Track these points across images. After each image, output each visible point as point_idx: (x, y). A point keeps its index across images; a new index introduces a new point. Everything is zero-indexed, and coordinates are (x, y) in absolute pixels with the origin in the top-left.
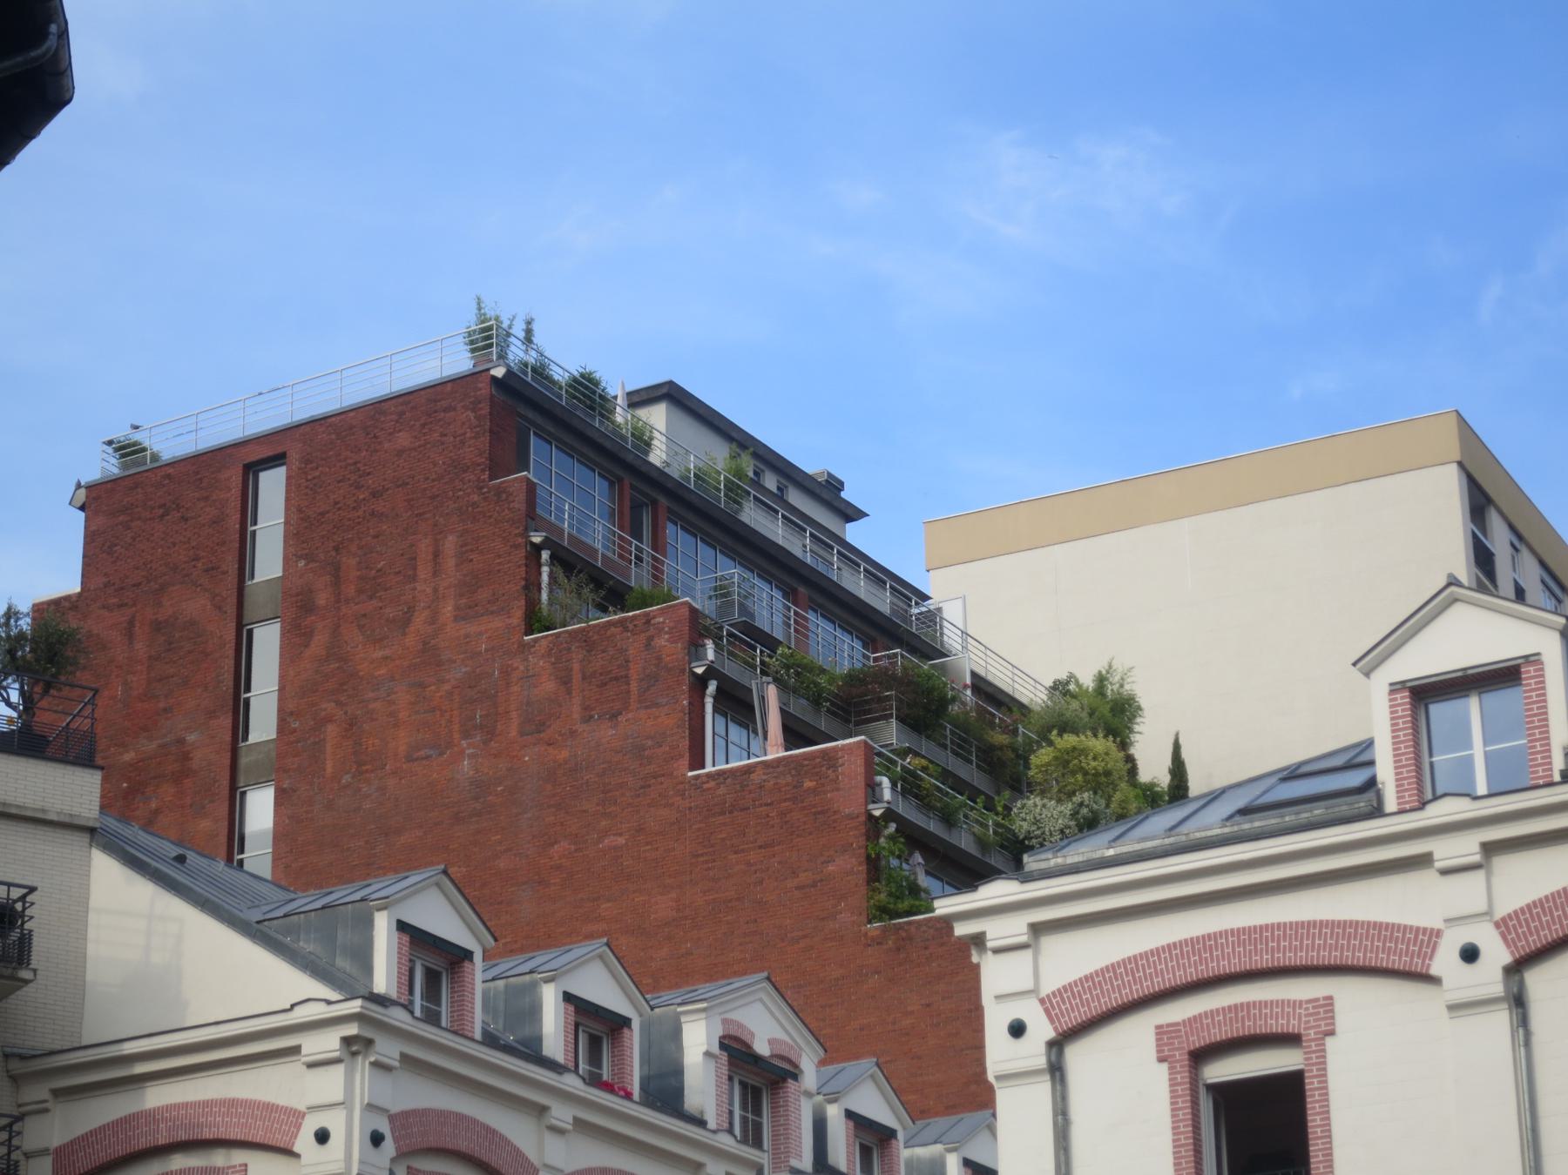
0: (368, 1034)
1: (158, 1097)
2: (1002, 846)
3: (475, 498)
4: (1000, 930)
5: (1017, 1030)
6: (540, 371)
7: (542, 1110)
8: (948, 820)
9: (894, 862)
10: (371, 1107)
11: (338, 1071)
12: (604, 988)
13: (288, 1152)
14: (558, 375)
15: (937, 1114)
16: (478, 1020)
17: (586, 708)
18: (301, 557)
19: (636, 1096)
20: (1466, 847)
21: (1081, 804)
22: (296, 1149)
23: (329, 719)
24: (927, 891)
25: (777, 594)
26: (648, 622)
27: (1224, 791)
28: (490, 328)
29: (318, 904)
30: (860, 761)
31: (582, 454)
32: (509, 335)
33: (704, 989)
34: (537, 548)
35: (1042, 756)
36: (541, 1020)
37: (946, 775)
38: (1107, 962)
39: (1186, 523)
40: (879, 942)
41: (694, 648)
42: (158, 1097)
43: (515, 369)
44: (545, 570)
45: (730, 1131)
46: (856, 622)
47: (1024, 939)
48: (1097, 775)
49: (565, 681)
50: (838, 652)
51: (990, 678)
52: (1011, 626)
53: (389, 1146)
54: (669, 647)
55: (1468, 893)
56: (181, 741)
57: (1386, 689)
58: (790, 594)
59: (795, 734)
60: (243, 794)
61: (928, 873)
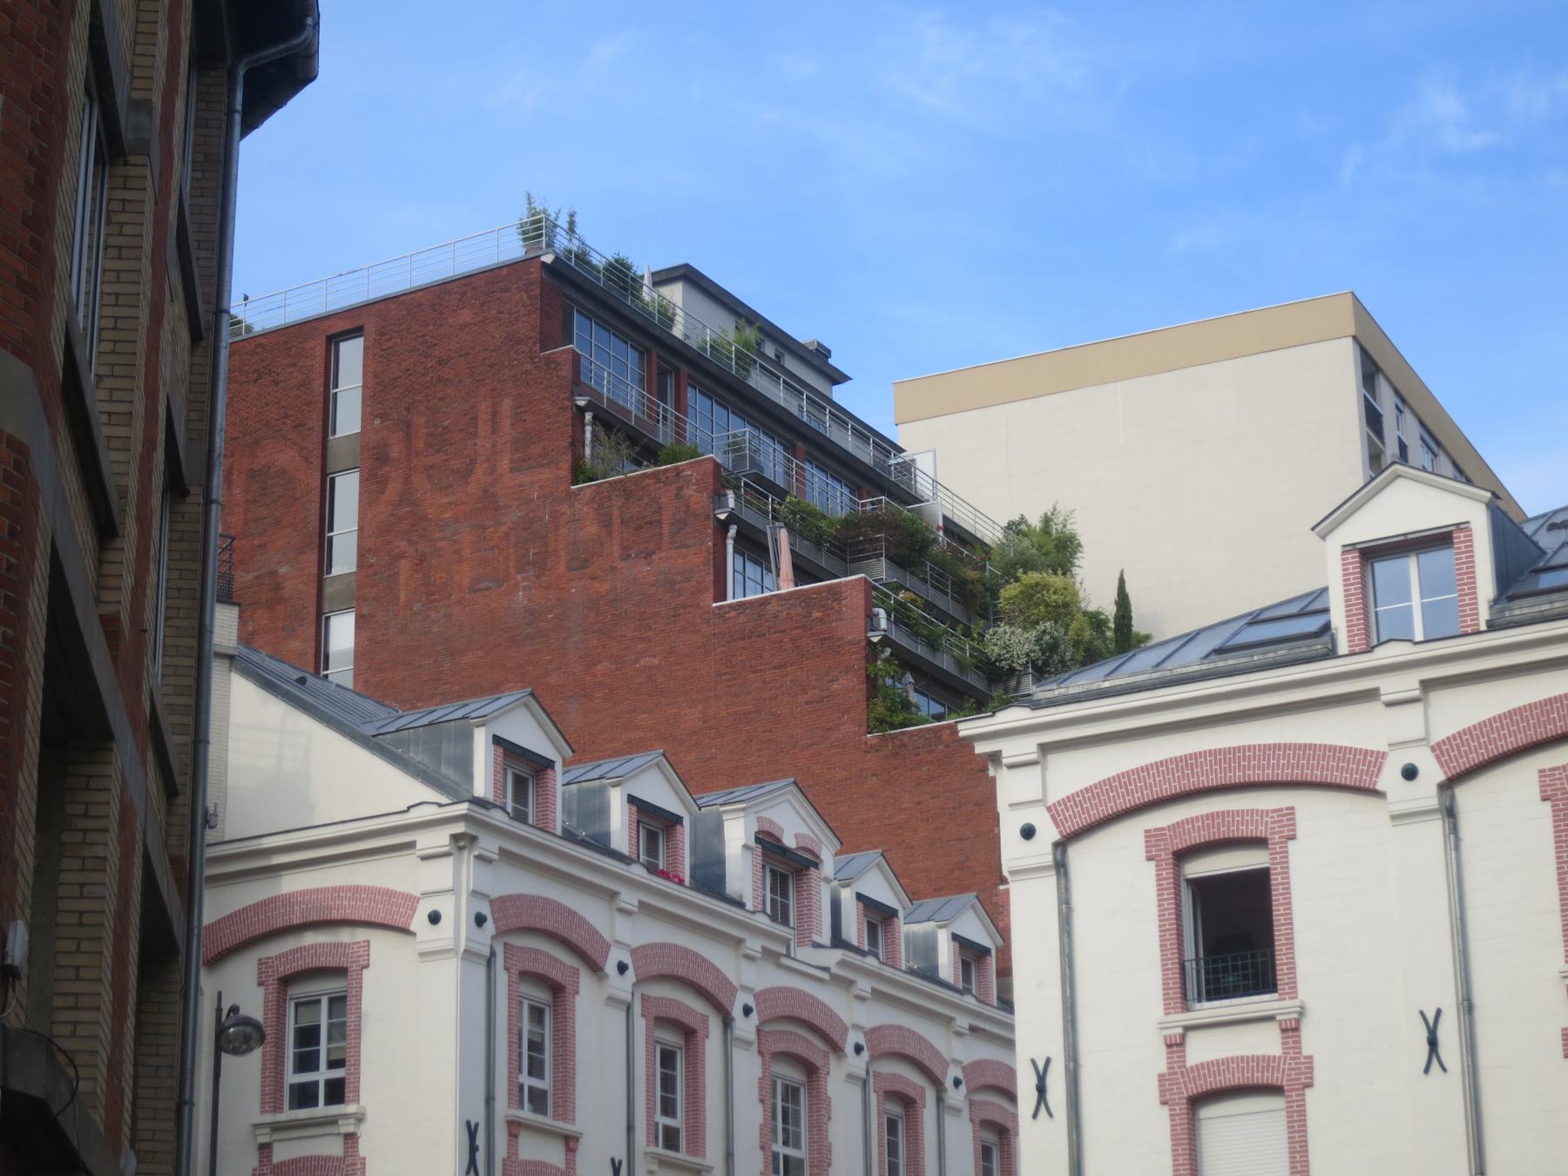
0: (473, 832)
1: (291, 884)
2: (977, 667)
3: (528, 367)
4: (1012, 750)
5: (1028, 833)
6: (582, 257)
7: (613, 895)
8: (933, 645)
9: (889, 681)
10: (475, 894)
11: (448, 863)
12: (661, 792)
13: (405, 931)
14: (597, 260)
15: (926, 896)
16: (559, 821)
17: (624, 548)
18: (377, 416)
19: (687, 882)
20: (1407, 684)
21: (1044, 632)
22: (412, 928)
23: (402, 556)
24: (917, 707)
25: (779, 448)
26: (678, 475)
27: (1198, 633)
28: (540, 221)
29: (426, 721)
30: (861, 595)
31: (616, 329)
32: (556, 226)
33: (740, 792)
34: (582, 410)
35: (1009, 591)
36: (609, 819)
37: (929, 606)
38: (1105, 777)
39: (1119, 385)
40: (876, 749)
41: (718, 498)
42: (291, 884)
43: (561, 255)
44: (588, 429)
45: (764, 912)
46: (845, 473)
47: (1034, 757)
48: (1057, 606)
49: (607, 525)
50: (830, 498)
51: (956, 520)
52: (973, 476)
53: (490, 926)
54: (696, 496)
55: (1408, 722)
56: (274, 574)
57: (1340, 550)
58: (790, 448)
59: (803, 572)
60: (328, 618)
61: (916, 690)
